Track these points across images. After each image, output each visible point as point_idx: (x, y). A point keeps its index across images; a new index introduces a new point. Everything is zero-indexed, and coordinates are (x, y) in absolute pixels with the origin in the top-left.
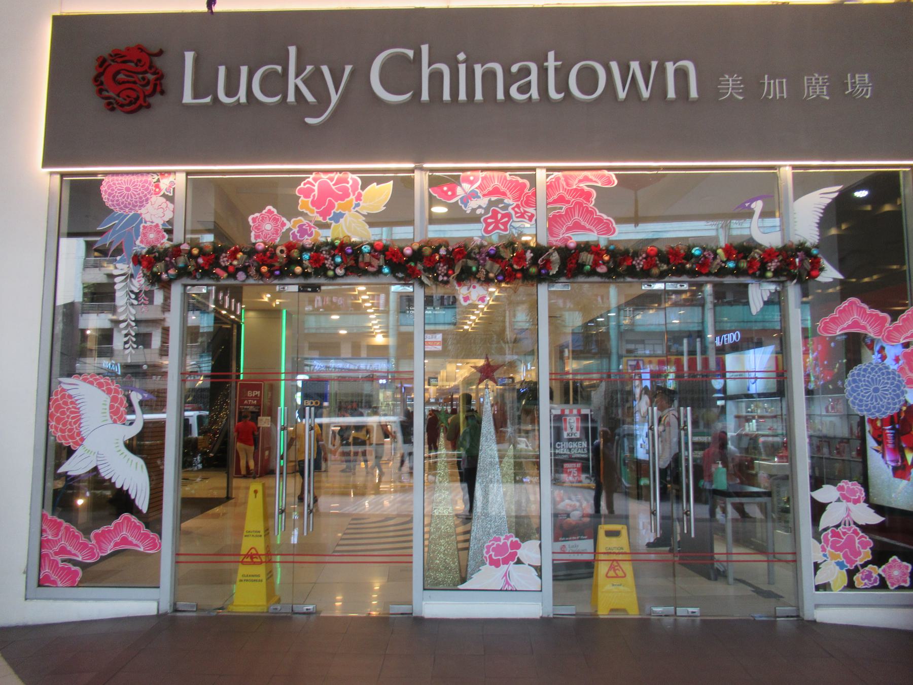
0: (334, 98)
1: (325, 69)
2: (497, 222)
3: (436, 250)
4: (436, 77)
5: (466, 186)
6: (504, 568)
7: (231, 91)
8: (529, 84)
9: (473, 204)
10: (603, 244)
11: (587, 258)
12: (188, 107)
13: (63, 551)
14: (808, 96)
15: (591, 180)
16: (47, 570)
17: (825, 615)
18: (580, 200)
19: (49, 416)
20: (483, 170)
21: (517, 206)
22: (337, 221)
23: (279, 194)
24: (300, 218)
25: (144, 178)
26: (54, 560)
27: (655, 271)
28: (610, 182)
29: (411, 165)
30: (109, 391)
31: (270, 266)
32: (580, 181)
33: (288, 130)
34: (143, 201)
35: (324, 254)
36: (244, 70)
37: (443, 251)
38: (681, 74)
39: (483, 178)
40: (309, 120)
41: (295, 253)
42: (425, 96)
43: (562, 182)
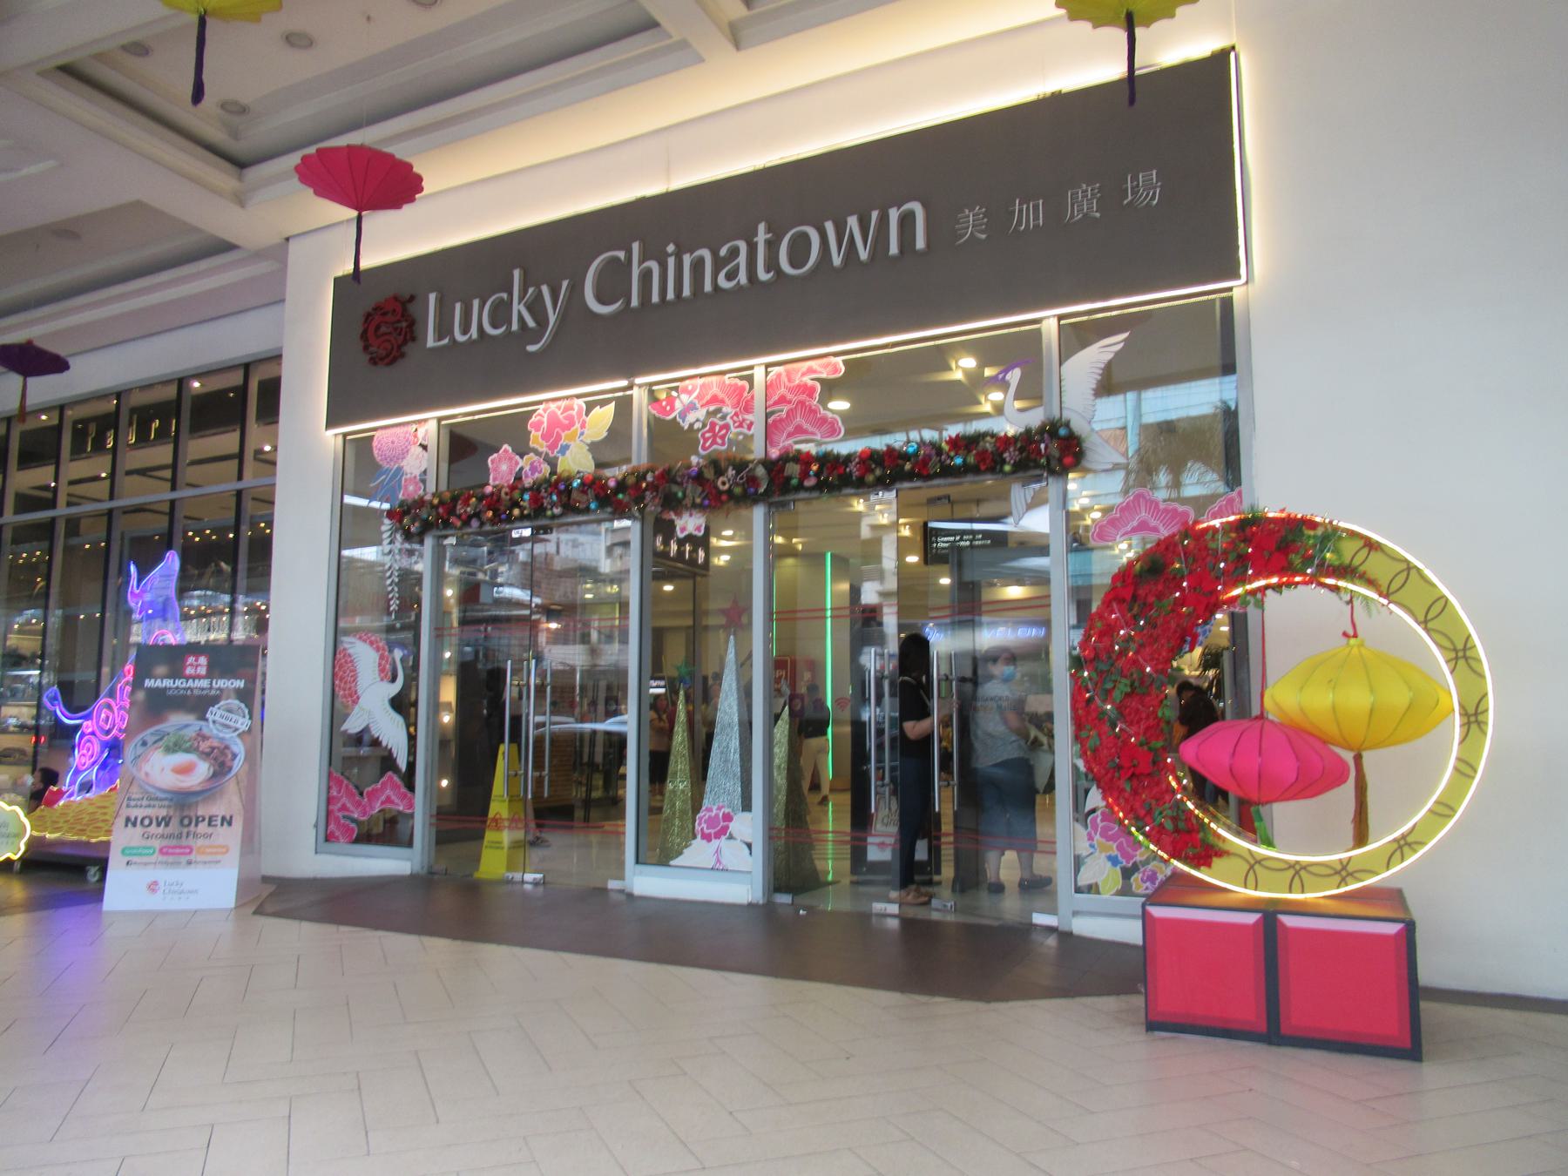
0: (552, 319)
2: (715, 436)
3: (643, 477)
4: (646, 276)
5: (684, 397)
6: (715, 843)
8: (737, 268)
9: (691, 418)
10: (814, 452)
11: (793, 469)
12: (433, 349)
13: (344, 808)
14: (1072, 216)
15: (815, 372)
16: (332, 827)
17: (1085, 927)
18: (803, 397)
19: (334, 675)
20: (701, 376)
21: (736, 414)
23: (515, 429)
25: (405, 429)
27: (870, 478)
28: (836, 370)
29: (624, 383)
30: (378, 649)
31: (496, 511)
32: (804, 374)
33: (511, 363)
34: (404, 453)
35: (543, 493)
36: (476, 303)
37: (649, 478)
38: (907, 221)
39: (703, 386)
40: (531, 348)
41: (516, 494)
42: (635, 302)
43: (784, 379)
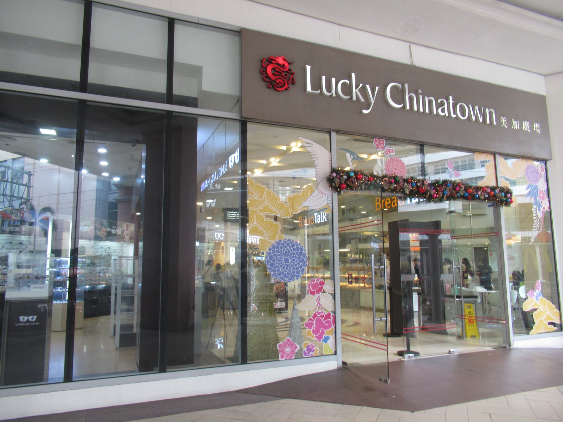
0: (373, 102)
1: (368, 86)
7: (329, 89)
22: (326, 342)
24: (307, 342)
26: (260, 216)
